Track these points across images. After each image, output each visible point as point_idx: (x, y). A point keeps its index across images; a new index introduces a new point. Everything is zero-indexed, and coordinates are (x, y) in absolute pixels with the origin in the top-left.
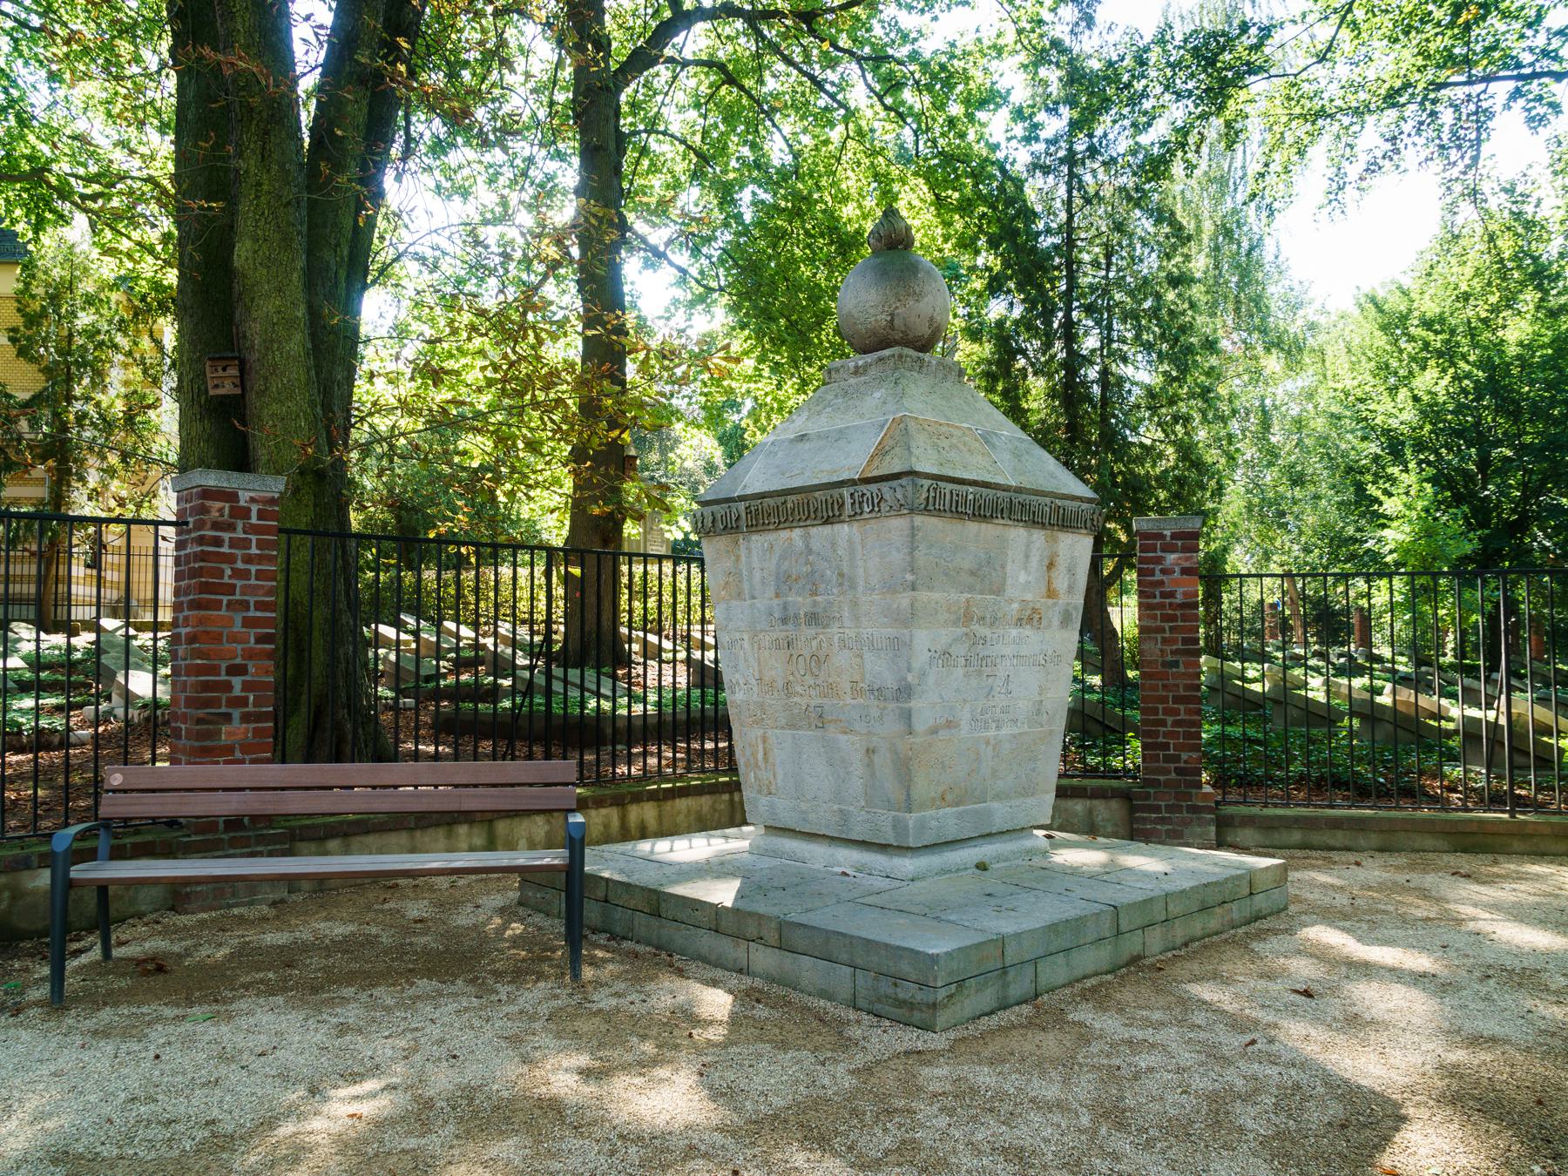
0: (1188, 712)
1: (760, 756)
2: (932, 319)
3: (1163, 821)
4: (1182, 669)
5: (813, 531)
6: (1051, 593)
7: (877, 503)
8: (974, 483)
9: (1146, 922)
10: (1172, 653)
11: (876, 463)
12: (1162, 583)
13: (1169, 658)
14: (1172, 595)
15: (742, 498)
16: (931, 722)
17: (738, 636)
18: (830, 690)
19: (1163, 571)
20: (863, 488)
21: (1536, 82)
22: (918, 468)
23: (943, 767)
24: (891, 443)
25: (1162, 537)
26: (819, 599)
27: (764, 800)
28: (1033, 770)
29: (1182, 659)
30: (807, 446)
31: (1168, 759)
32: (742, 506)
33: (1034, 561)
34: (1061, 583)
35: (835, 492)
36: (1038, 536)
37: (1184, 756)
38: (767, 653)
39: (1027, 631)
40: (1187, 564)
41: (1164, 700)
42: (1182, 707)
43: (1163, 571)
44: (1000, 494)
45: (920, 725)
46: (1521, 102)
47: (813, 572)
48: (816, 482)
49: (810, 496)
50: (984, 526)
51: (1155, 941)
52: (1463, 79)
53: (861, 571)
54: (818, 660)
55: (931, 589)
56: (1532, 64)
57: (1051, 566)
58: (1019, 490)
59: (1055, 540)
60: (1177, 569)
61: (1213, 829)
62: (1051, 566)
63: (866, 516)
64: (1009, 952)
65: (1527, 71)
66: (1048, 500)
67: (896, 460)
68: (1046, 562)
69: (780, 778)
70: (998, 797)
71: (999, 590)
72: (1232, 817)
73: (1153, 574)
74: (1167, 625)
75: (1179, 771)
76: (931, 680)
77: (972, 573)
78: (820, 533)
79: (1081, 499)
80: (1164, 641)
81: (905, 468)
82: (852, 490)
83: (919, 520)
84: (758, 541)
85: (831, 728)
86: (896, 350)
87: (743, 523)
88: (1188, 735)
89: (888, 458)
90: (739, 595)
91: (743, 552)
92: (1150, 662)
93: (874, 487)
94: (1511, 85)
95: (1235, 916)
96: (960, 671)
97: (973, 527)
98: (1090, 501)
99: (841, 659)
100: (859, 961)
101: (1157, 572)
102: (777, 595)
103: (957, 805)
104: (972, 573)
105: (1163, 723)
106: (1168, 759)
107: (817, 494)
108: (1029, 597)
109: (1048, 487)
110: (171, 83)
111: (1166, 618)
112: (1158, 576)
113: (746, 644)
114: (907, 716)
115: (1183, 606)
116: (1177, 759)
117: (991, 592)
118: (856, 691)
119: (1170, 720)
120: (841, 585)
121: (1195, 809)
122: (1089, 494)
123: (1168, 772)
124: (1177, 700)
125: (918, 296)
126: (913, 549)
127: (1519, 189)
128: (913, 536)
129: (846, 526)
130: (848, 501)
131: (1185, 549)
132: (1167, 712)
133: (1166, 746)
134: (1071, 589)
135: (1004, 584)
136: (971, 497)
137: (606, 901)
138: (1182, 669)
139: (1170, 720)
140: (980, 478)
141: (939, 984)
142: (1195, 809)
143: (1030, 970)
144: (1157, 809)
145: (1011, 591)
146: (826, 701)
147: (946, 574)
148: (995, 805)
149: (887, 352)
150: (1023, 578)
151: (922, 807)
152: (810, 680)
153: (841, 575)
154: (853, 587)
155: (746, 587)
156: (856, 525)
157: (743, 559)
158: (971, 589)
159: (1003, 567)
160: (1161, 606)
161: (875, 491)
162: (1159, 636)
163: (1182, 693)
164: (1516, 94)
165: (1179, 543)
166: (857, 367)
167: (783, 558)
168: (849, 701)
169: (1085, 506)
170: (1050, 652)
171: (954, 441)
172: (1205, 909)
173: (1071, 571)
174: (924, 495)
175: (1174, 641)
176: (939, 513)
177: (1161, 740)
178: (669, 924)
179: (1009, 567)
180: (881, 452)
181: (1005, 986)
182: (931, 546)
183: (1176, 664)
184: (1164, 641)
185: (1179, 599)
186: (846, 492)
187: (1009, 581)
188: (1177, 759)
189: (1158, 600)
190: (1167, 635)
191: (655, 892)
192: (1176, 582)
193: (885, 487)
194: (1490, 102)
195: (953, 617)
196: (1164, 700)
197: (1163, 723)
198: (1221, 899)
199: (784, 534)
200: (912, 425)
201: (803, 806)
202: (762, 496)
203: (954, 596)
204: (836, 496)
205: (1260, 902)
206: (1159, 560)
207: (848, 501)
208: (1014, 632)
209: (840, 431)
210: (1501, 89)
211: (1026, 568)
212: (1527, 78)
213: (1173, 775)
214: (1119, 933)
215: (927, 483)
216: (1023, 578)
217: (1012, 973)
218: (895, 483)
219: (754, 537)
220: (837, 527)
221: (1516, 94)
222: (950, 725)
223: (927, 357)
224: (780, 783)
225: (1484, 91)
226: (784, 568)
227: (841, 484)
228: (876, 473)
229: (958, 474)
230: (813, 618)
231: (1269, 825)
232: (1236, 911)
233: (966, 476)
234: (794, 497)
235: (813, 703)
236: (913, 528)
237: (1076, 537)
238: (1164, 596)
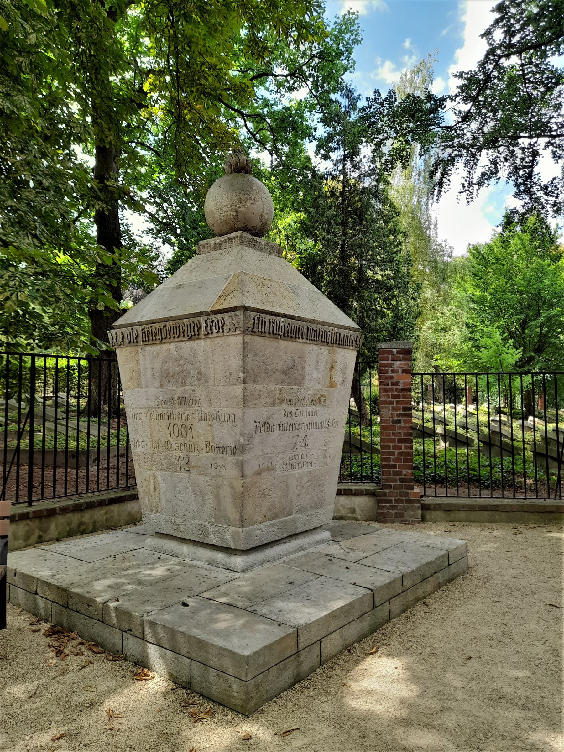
0: (406, 447)
1: (152, 487)
2: (261, 216)
3: (393, 508)
4: (403, 424)
5: (183, 344)
6: (332, 385)
7: (221, 327)
8: (285, 316)
9: (391, 596)
10: (398, 415)
11: (221, 301)
12: (392, 377)
13: (396, 418)
14: (397, 384)
15: (140, 324)
16: (256, 468)
17: (138, 411)
18: (192, 447)
19: (393, 371)
20: (212, 317)
21: (557, 139)
22: (248, 304)
23: (265, 496)
24: (232, 288)
25: (391, 352)
26: (186, 388)
27: (153, 516)
28: (322, 492)
29: (402, 419)
30: (182, 290)
31: (396, 474)
32: (140, 328)
33: (322, 366)
34: (338, 378)
35: (196, 320)
36: (325, 350)
37: (404, 472)
38: (156, 421)
39: (318, 407)
40: (406, 368)
41: (393, 441)
42: (403, 445)
43: (393, 371)
44: (301, 323)
45: (249, 471)
46: (551, 148)
47: (182, 371)
48: (184, 313)
49: (180, 322)
50: (291, 343)
51: (396, 606)
52: (527, 135)
53: (211, 370)
54: (187, 428)
55: (256, 382)
56: (556, 130)
57: (332, 368)
58: (313, 322)
59: (335, 353)
60: (400, 370)
61: (420, 512)
62: (332, 368)
63: (215, 335)
64: (302, 639)
65: (554, 133)
66: (330, 328)
67: (234, 299)
68: (329, 365)
69: (163, 502)
70: (300, 511)
71: (299, 383)
72: (429, 505)
73: (387, 373)
74: (395, 401)
75: (401, 480)
76: (256, 441)
77: (284, 372)
78: (187, 346)
79: (350, 329)
80: (394, 409)
81: (239, 304)
82: (206, 318)
83: (248, 338)
84: (150, 349)
85: (194, 471)
86: (238, 233)
87: (140, 339)
88: (406, 460)
89: (229, 298)
90: (139, 385)
91: (141, 357)
92: (386, 420)
93: (219, 316)
94: (547, 139)
95: (441, 580)
96: (277, 432)
97: (284, 344)
98: (355, 330)
99: (200, 427)
100: (194, 655)
101: (390, 372)
102: (162, 385)
103: (274, 519)
104: (284, 372)
105: (393, 454)
106: (396, 474)
107: (185, 321)
108: (318, 386)
109: (330, 321)
110: (95, 227)
111: (394, 397)
112: (390, 374)
113: (143, 416)
114: (241, 465)
115: (403, 390)
116: (400, 473)
117: (296, 384)
118: (209, 448)
119: (396, 452)
120: (200, 379)
121: (409, 501)
122: (356, 326)
123: (396, 481)
124: (400, 441)
125: (254, 201)
126: (245, 356)
127: (549, 189)
128: (244, 348)
129: (202, 341)
130: (204, 325)
131: (404, 359)
132: (395, 447)
133: (394, 466)
134: (344, 381)
135: (303, 378)
136: (282, 324)
137: (36, 594)
138: (403, 424)
139: (396, 452)
140: (288, 313)
141: (249, 678)
142: (409, 501)
143: (317, 646)
144: (390, 501)
145: (307, 384)
146: (190, 453)
147: (266, 373)
148: (299, 516)
149: (233, 235)
150: (315, 375)
151: (253, 523)
152: (181, 440)
153: (200, 373)
154: (207, 381)
155: (143, 381)
156: (209, 341)
157: (141, 362)
158: (283, 382)
159: (303, 368)
160: (392, 390)
161: (220, 319)
162: (390, 406)
163: (403, 437)
164: (548, 144)
165: (401, 356)
166: (215, 244)
167: (165, 362)
168: (205, 454)
169: (352, 333)
170: (331, 420)
171: (273, 290)
172: (424, 579)
173: (344, 371)
174: (251, 322)
175: (398, 409)
176: (262, 334)
177: (392, 463)
178: (74, 614)
179: (307, 368)
180: (226, 294)
181: (299, 665)
182: (256, 355)
183: (399, 422)
184: (394, 409)
185: (401, 386)
186: (202, 320)
187: (307, 378)
188: (400, 473)
189: (390, 387)
190: (395, 405)
191: (65, 590)
192: (399, 377)
193: (226, 316)
194: (538, 147)
195: (270, 401)
196: (393, 441)
197: (393, 454)
198: (433, 571)
199: (166, 346)
200: (246, 279)
201: (178, 521)
202: (153, 322)
203: (272, 387)
204: (196, 322)
205: (454, 569)
206: (390, 365)
207: (204, 325)
208: (310, 409)
209: (202, 282)
210: (543, 141)
211: (317, 369)
212: (554, 137)
213: (398, 483)
214: (374, 607)
215: (253, 314)
216: (315, 375)
217: (304, 654)
218: (232, 314)
219: (148, 348)
220: (198, 342)
221: (548, 144)
222: (270, 469)
223: (258, 239)
224: (164, 506)
225: (536, 142)
226: (165, 368)
227: (201, 314)
228: (221, 307)
229: (274, 310)
230: (183, 401)
231: (448, 509)
232: (442, 577)
233: (279, 311)
234: (171, 323)
235: (182, 455)
236: (244, 342)
237: (346, 351)
238: (393, 384)
